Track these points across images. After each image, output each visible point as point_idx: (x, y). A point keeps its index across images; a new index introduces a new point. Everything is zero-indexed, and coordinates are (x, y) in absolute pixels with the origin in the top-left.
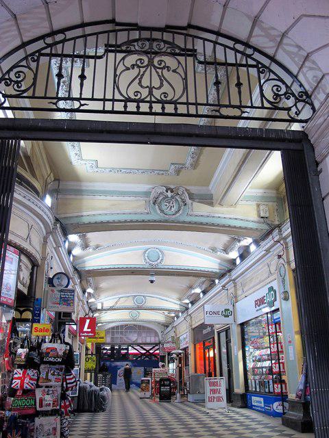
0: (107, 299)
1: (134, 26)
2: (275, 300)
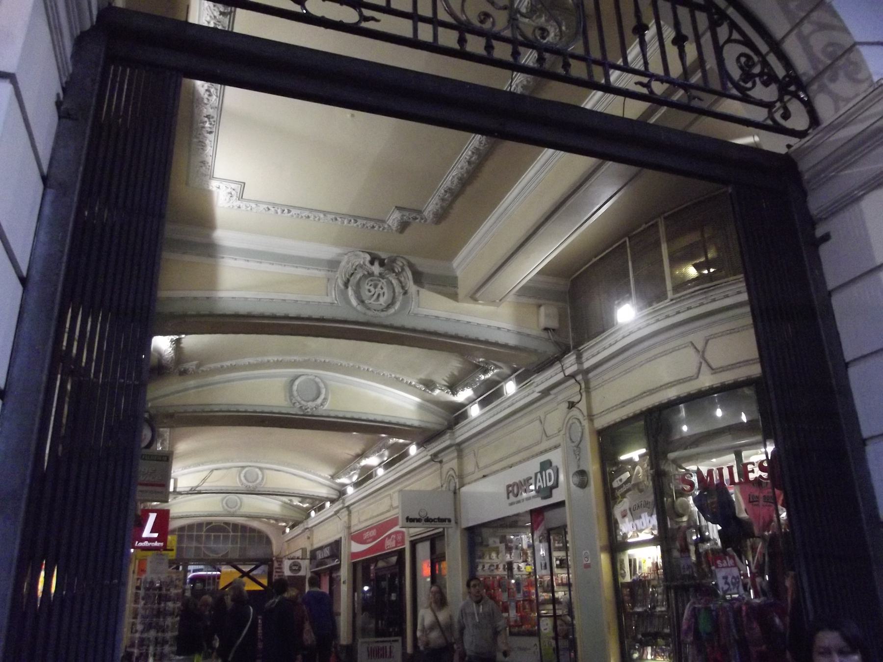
0: (186, 471)
2: (556, 485)
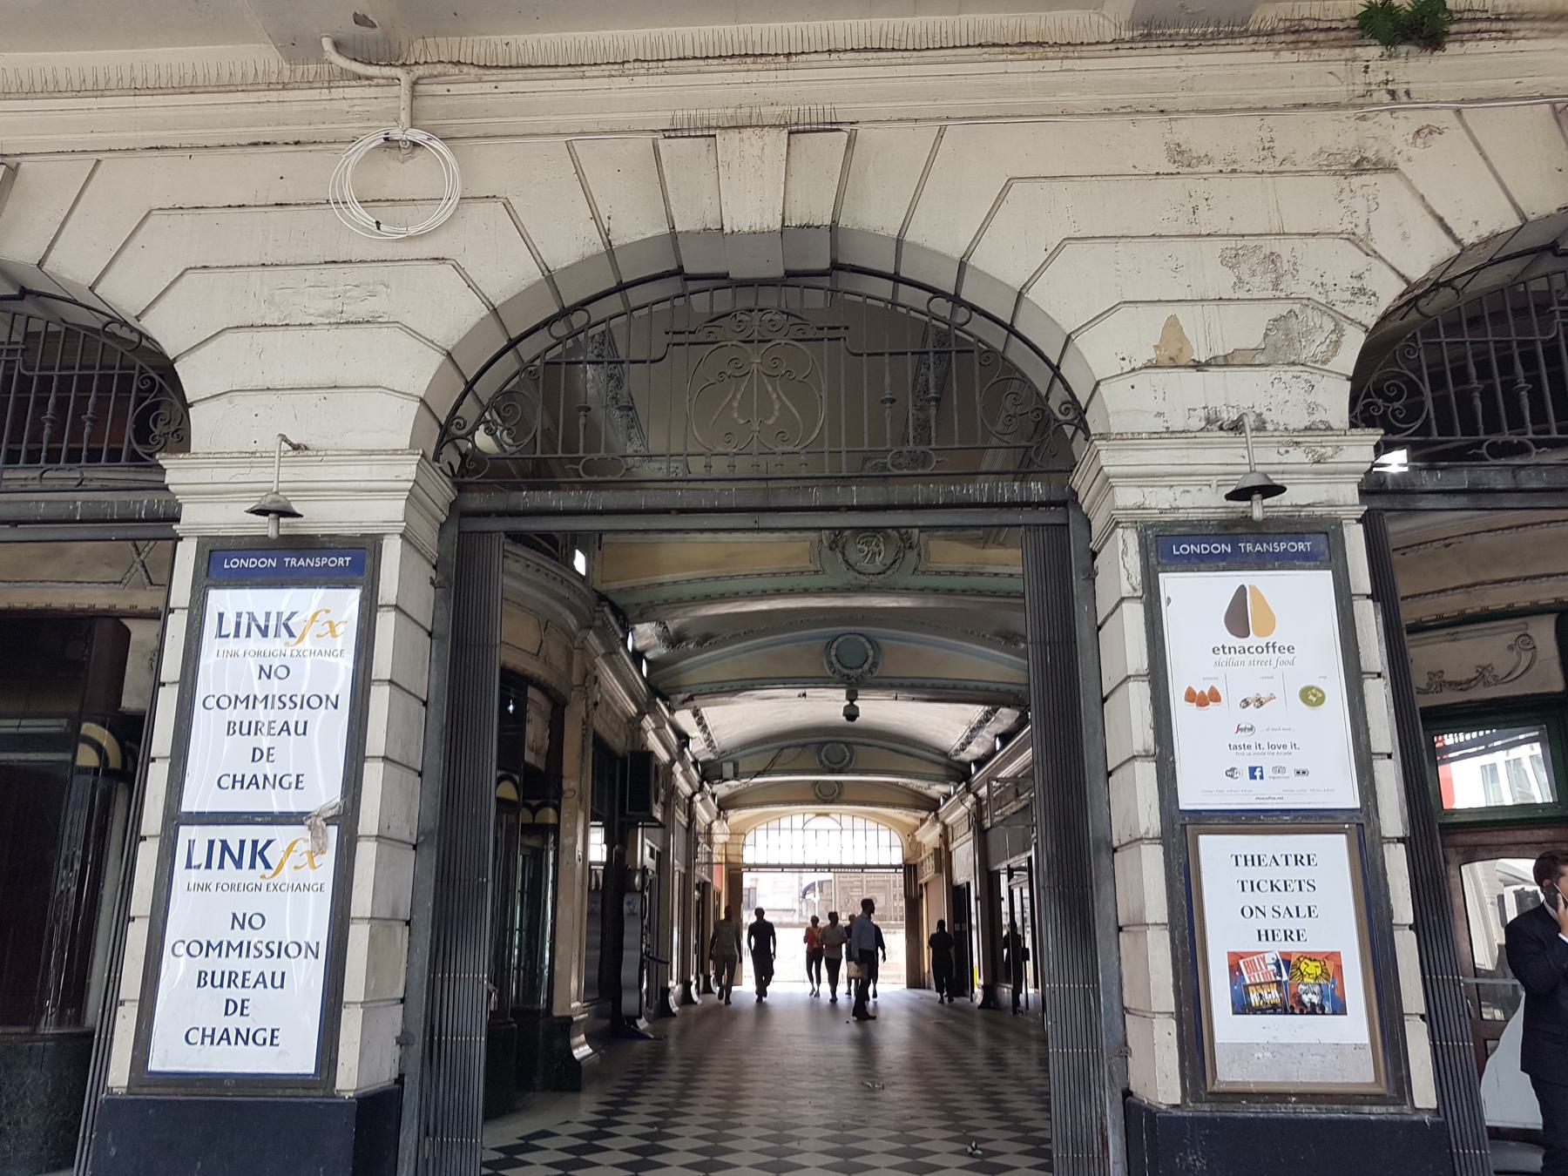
1: (721, 280)
